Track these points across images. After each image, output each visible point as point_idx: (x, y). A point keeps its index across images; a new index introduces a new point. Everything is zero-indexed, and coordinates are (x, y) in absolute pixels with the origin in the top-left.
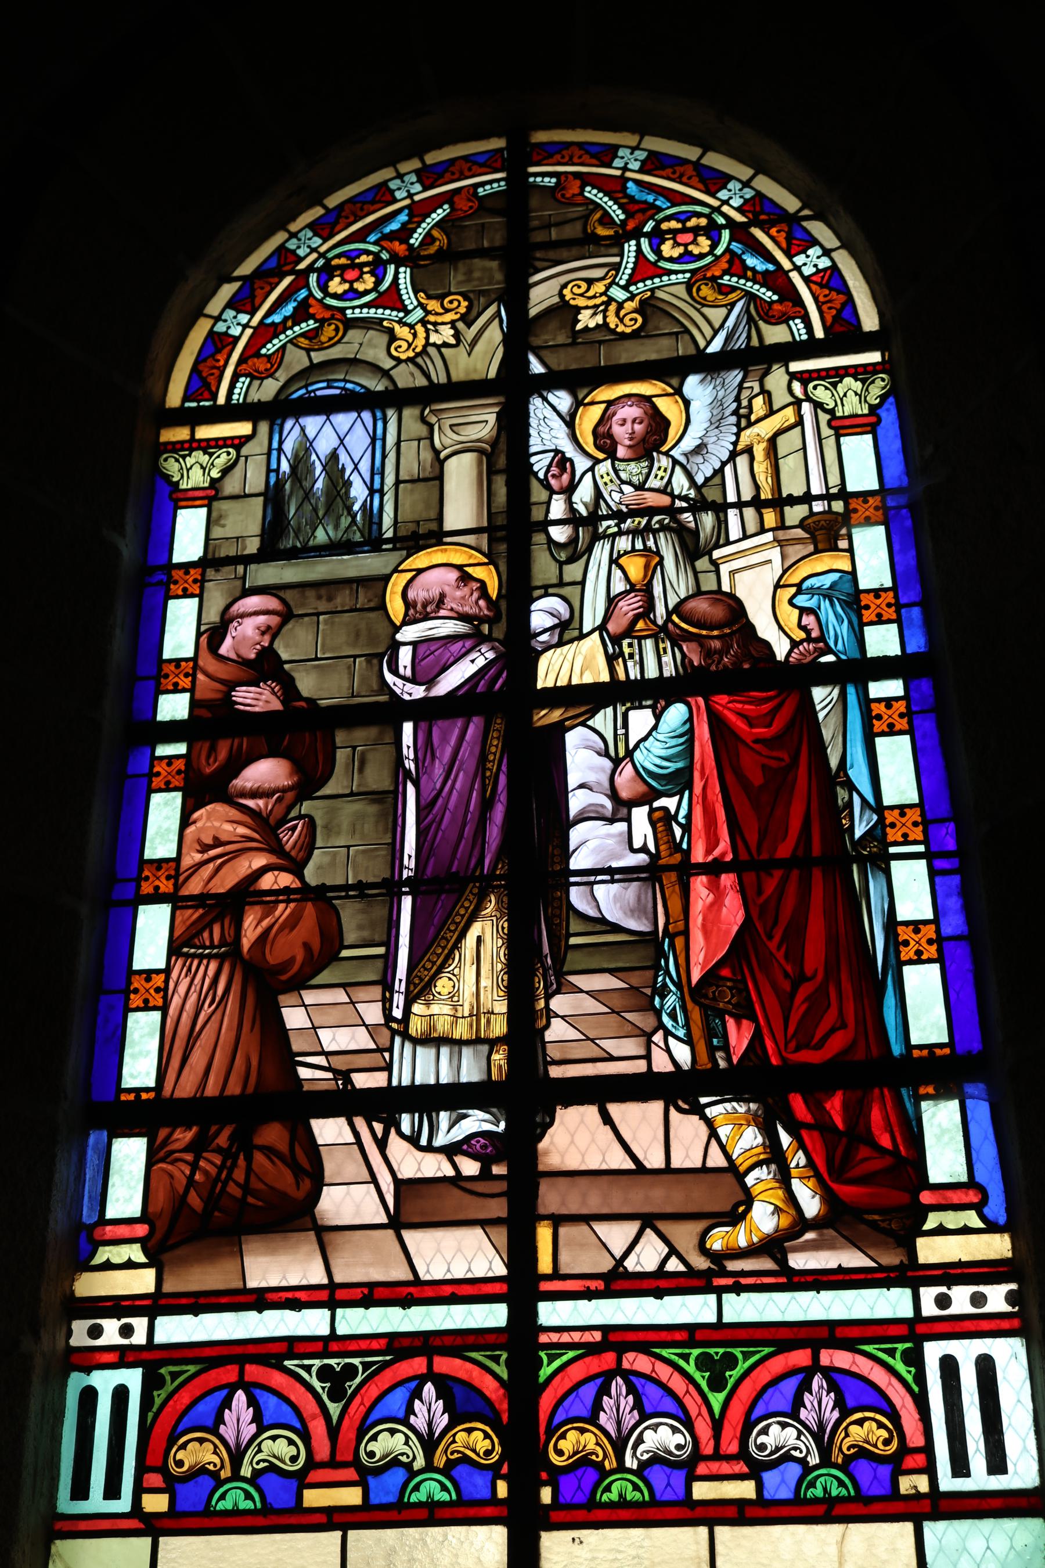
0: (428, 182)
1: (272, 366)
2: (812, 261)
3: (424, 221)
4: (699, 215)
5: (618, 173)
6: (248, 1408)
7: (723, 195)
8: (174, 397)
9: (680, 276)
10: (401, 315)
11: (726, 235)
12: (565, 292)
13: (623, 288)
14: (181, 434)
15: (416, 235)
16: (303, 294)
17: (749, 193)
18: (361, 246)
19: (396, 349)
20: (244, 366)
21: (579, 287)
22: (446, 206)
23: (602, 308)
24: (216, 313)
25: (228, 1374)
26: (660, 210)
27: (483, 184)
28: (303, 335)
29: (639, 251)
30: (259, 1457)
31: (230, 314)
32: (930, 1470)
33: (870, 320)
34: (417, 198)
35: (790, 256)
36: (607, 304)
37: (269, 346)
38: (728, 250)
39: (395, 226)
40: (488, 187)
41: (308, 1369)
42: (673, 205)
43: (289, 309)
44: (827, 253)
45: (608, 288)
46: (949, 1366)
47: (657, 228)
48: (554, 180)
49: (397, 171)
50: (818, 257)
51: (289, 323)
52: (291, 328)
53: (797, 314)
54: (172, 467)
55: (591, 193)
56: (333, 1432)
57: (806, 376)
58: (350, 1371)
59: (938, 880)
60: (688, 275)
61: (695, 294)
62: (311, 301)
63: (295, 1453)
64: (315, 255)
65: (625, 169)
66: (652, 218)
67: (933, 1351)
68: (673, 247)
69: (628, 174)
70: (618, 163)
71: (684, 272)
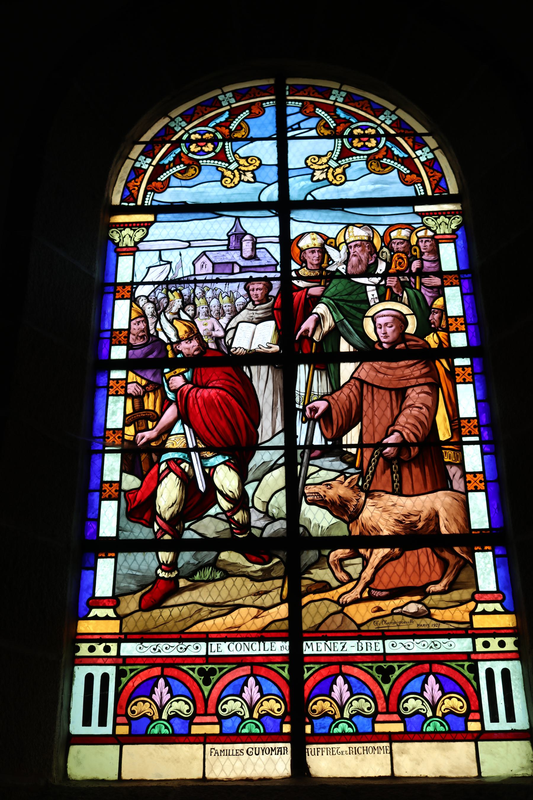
0: (238, 98)
1: (164, 187)
2: (424, 155)
3: (237, 118)
4: (372, 128)
5: (332, 103)
6: (345, 684)
7: (382, 117)
8: (116, 200)
9: (362, 157)
10: (227, 165)
11: (383, 140)
12: (308, 161)
13: (335, 161)
15: (232, 125)
16: (178, 151)
17: (394, 118)
18: (207, 129)
20: (150, 186)
21: (315, 159)
22: (247, 111)
23: (326, 170)
24: (135, 158)
26: (353, 123)
27: (265, 101)
28: (179, 172)
29: (343, 143)
30: (171, 709)
31: (142, 158)
32: (481, 720)
33: (453, 189)
34: (233, 106)
35: (414, 150)
38: (385, 145)
39: (222, 119)
40: (268, 103)
41: (131, 671)
42: (359, 122)
43: (171, 158)
44: (432, 151)
45: (328, 161)
46: (490, 673)
47: (351, 132)
49: (222, 91)
50: (428, 153)
51: (172, 165)
52: (172, 168)
53: (419, 181)
55: (319, 111)
56: (387, 699)
57: (424, 214)
58: (213, 672)
59: (485, 457)
60: (366, 157)
61: (369, 166)
62: (182, 154)
63: (369, 706)
64: (183, 132)
65: (335, 101)
66: (349, 127)
67: (108, 730)
68: (359, 142)
69: (337, 104)
70: (332, 98)
71: (363, 155)
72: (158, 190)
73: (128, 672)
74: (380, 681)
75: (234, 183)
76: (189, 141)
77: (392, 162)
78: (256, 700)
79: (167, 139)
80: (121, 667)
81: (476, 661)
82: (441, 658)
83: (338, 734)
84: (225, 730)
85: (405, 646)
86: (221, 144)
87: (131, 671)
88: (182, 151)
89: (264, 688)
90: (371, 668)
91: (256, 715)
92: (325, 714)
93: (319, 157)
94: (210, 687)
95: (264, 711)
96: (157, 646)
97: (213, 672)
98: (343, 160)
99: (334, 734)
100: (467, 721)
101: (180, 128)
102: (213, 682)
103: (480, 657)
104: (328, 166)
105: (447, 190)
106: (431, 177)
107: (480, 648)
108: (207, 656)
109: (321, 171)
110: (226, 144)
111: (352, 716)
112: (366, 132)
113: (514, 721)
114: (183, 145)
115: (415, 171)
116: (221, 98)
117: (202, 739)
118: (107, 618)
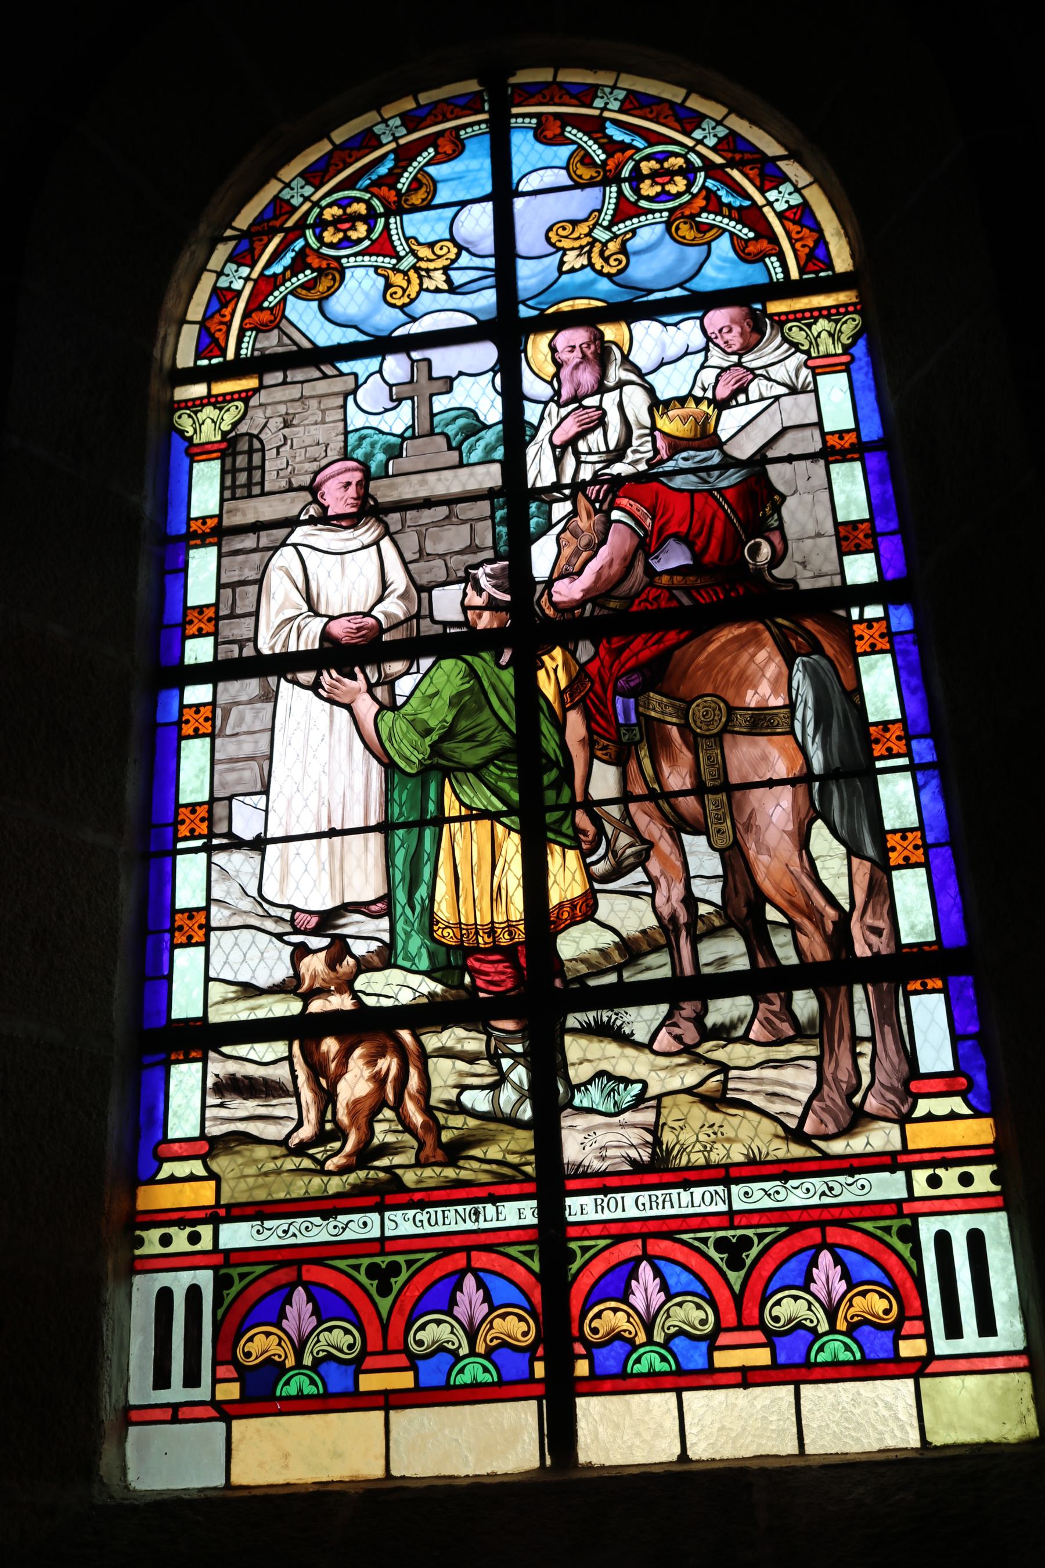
1: (275, 318)
2: (782, 198)
3: (410, 165)
4: (676, 155)
5: (597, 112)
6: (478, 1290)
7: (698, 134)
10: (394, 261)
11: (701, 175)
12: (551, 234)
14: (199, 390)
15: (403, 180)
16: (299, 244)
17: (722, 132)
19: (391, 295)
21: (564, 229)
22: (431, 150)
25: (814, 1235)
26: (638, 150)
27: (464, 127)
28: (302, 286)
29: (620, 192)
32: (927, 1335)
33: (842, 262)
34: (402, 142)
35: (763, 191)
36: (592, 244)
37: (271, 298)
38: (703, 187)
39: (383, 170)
40: (469, 130)
42: (651, 145)
43: (287, 260)
45: (591, 230)
46: (943, 1240)
47: (636, 169)
48: (534, 121)
50: (790, 194)
52: (289, 280)
54: (185, 423)
55: (571, 132)
56: (738, 1299)
57: (783, 318)
62: (307, 250)
63: (351, 1341)
64: (307, 206)
65: (605, 109)
66: (631, 158)
67: (202, 1393)
68: (652, 186)
69: (606, 114)
72: (267, 325)
73: (404, 1266)
74: (725, 1268)
75: (409, 296)
76: (321, 225)
77: (719, 218)
78: (480, 1318)
79: (277, 223)
80: (222, 1271)
81: (915, 1217)
82: (846, 1214)
83: (465, 1386)
84: (424, 1382)
85: (769, 1195)
86: (381, 222)
87: (887, 1230)
88: (307, 244)
89: (671, 1282)
90: (887, 1230)
91: (842, 1325)
92: (618, 1336)
93: (575, 223)
94: (390, 1298)
95: (858, 1316)
96: (290, 1224)
97: (394, 1269)
98: (621, 226)
99: (456, 1387)
100: (898, 1337)
101: (301, 200)
102: (396, 1289)
103: (926, 1206)
104: (590, 240)
105: (830, 266)
106: (797, 240)
107: (921, 1189)
108: (383, 1239)
109: (576, 252)
110: (392, 220)
111: (669, 1338)
112: (666, 165)
113: (994, 1333)
114: (309, 233)
115: (765, 232)
116: (378, 129)
117: (381, 1400)
118: (192, 1178)
